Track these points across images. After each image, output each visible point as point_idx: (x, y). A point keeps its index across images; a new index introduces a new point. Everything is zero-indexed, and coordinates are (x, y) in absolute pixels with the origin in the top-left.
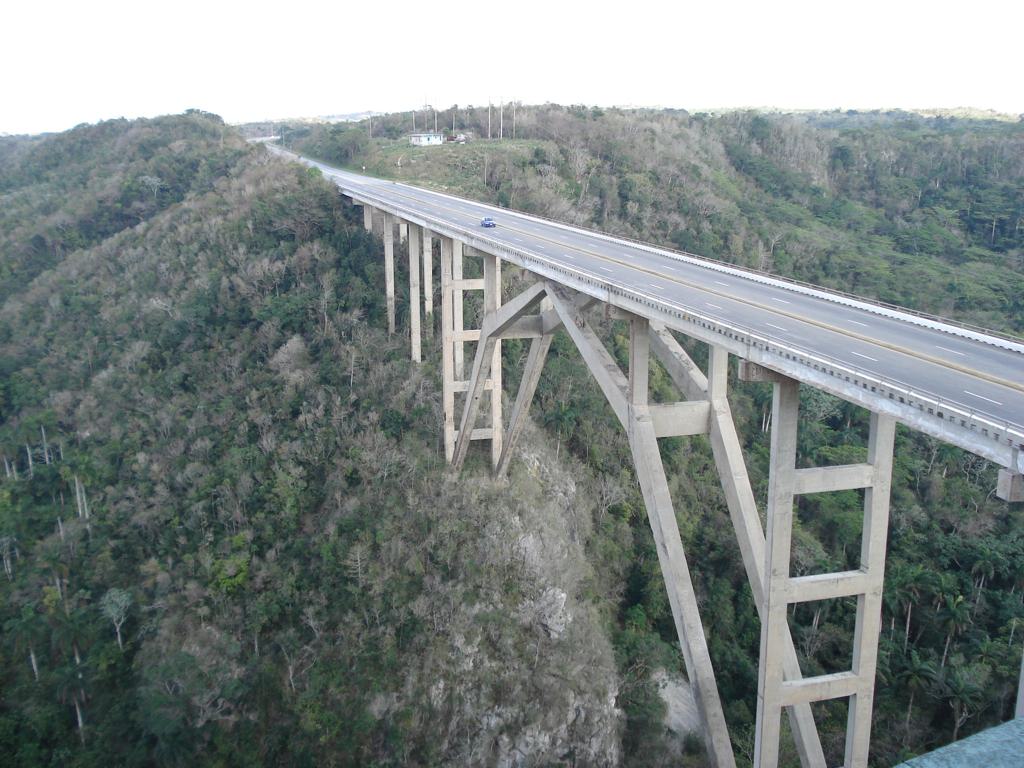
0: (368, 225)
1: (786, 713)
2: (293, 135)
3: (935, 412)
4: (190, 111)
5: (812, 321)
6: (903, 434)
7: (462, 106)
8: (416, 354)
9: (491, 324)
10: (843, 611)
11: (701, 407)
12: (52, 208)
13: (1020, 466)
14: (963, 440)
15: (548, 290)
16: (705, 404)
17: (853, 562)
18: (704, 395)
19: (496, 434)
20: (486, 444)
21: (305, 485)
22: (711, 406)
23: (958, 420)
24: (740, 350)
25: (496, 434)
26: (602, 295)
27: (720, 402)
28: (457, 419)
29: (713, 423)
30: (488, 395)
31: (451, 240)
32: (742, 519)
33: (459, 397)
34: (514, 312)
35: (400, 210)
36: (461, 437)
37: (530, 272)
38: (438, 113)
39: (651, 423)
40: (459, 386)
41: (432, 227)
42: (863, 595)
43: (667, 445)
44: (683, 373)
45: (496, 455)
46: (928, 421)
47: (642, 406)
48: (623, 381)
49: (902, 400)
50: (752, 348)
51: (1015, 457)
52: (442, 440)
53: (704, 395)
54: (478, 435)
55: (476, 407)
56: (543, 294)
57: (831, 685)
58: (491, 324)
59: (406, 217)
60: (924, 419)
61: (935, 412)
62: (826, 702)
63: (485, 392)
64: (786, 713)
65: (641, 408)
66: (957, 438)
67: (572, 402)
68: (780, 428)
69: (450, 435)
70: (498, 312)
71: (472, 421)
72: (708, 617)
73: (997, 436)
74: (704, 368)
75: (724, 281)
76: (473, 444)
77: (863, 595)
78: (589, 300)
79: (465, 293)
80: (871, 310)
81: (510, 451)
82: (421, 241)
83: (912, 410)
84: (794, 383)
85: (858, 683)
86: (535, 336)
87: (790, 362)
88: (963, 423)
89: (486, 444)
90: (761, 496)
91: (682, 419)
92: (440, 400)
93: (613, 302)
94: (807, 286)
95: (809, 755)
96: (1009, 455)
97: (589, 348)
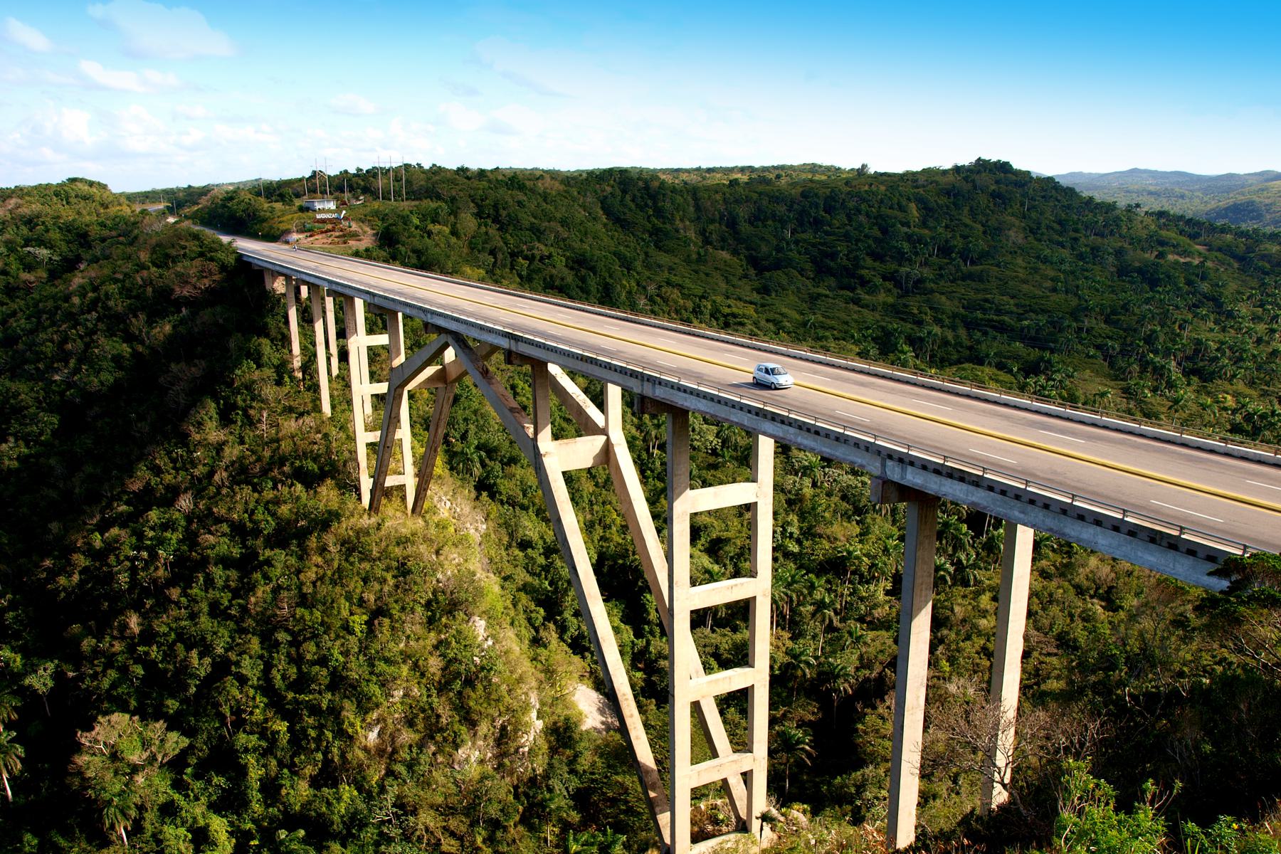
1: (696, 707)
2: (180, 200)
3: (812, 431)
4: (73, 180)
7: (352, 171)
10: (742, 611)
12: (1042, 365)
13: (888, 473)
14: (837, 454)
15: (450, 340)
17: (753, 574)
21: (255, 517)
22: (608, 440)
29: (611, 454)
31: (318, 286)
38: (329, 176)
43: (569, 477)
46: (807, 439)
50: (646, 383)
51: (884, 465)
54: (390, 481)
56: (446, 346)
57: (734, 679)
59: (307, 279)
60: (803, 438)
61: (812, 431)
64: (696, 707)
66: (833, 452)
67: (453, 607)
69: (366, 484)
78: (488, 349)
79: (370, 349)
83: (792, 430)
85: (756, 677)
89: (402, 488)
90: (663, 521)
93: (514, 349)
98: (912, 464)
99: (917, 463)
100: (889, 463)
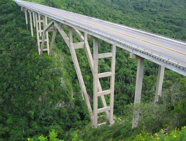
0: (22, 10)
5: (172, 49)
6: (117, 47)
8: (32, 35)
9: (45, 29)
11: (82, 43)
16: (84, 42)
18: (84, 41)
19: (48, 49)
20: (46, 52)
22: (85, 43)
23: (175, 65)
24: (169, 67)
25: (48, 49)
26: (63, 23)
27: (86, 42)
28: (40, 47)
30: (46, 42)
32: (91, 63)
33: (41, 43)
34: (50, 25)
35: (51, 16)
36: (41, 50)
37: (90, 35)
39: (73, 46)
40: (41, 41)
41: (135, 53)
42: (111, 76)
44: (80, 37)
45: (48, 53)
47: (72, 44)
48: (68, 39)
49: (114, 41)
52: (38, 51)
53: (84, 41)
54: (44, 50)
55: (44, 45)
57: (107, 92)
58: (45, 29)
62: (102, 89)
63: (45, 42)
65: (71, 44)
68: (95, 46)
69: (39, 50)
70: (47, 25)
71: (43, 47)
72: (85, 79)
73: (163, 61)
74: (84, 36)
75: (168, 43)
76: (44, 52)
77: (111, 76)
80: (180, 43)
81: (50, 54)
82: (38, 17)
84: (97, 38)
85: (111, 91)
86: (54, 31)
87: (143, 54)
88: (124, 45)
89: (46, 52)
91: (80, 45)
92: (37, 43)
94: (179, 41)
95: (102, 99)
96: (132, 50)
97: (62, 32)
98: (138, 51)
99: (139, 51)
100: (134, 50)
